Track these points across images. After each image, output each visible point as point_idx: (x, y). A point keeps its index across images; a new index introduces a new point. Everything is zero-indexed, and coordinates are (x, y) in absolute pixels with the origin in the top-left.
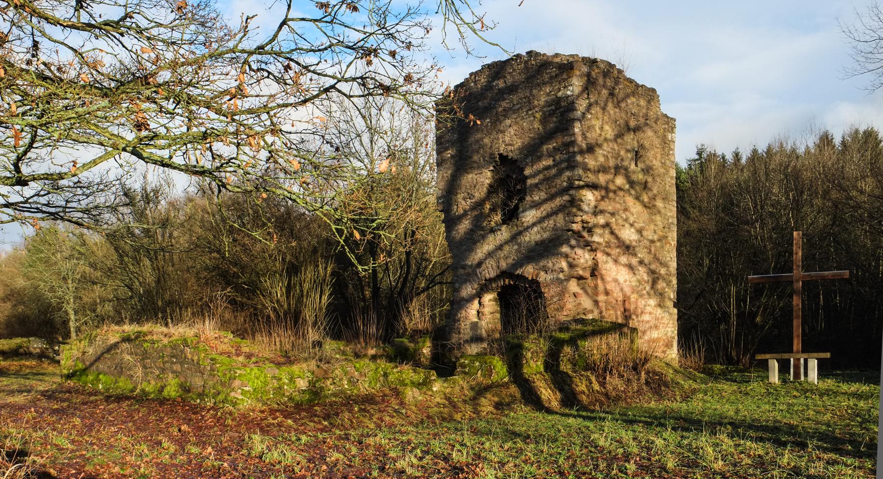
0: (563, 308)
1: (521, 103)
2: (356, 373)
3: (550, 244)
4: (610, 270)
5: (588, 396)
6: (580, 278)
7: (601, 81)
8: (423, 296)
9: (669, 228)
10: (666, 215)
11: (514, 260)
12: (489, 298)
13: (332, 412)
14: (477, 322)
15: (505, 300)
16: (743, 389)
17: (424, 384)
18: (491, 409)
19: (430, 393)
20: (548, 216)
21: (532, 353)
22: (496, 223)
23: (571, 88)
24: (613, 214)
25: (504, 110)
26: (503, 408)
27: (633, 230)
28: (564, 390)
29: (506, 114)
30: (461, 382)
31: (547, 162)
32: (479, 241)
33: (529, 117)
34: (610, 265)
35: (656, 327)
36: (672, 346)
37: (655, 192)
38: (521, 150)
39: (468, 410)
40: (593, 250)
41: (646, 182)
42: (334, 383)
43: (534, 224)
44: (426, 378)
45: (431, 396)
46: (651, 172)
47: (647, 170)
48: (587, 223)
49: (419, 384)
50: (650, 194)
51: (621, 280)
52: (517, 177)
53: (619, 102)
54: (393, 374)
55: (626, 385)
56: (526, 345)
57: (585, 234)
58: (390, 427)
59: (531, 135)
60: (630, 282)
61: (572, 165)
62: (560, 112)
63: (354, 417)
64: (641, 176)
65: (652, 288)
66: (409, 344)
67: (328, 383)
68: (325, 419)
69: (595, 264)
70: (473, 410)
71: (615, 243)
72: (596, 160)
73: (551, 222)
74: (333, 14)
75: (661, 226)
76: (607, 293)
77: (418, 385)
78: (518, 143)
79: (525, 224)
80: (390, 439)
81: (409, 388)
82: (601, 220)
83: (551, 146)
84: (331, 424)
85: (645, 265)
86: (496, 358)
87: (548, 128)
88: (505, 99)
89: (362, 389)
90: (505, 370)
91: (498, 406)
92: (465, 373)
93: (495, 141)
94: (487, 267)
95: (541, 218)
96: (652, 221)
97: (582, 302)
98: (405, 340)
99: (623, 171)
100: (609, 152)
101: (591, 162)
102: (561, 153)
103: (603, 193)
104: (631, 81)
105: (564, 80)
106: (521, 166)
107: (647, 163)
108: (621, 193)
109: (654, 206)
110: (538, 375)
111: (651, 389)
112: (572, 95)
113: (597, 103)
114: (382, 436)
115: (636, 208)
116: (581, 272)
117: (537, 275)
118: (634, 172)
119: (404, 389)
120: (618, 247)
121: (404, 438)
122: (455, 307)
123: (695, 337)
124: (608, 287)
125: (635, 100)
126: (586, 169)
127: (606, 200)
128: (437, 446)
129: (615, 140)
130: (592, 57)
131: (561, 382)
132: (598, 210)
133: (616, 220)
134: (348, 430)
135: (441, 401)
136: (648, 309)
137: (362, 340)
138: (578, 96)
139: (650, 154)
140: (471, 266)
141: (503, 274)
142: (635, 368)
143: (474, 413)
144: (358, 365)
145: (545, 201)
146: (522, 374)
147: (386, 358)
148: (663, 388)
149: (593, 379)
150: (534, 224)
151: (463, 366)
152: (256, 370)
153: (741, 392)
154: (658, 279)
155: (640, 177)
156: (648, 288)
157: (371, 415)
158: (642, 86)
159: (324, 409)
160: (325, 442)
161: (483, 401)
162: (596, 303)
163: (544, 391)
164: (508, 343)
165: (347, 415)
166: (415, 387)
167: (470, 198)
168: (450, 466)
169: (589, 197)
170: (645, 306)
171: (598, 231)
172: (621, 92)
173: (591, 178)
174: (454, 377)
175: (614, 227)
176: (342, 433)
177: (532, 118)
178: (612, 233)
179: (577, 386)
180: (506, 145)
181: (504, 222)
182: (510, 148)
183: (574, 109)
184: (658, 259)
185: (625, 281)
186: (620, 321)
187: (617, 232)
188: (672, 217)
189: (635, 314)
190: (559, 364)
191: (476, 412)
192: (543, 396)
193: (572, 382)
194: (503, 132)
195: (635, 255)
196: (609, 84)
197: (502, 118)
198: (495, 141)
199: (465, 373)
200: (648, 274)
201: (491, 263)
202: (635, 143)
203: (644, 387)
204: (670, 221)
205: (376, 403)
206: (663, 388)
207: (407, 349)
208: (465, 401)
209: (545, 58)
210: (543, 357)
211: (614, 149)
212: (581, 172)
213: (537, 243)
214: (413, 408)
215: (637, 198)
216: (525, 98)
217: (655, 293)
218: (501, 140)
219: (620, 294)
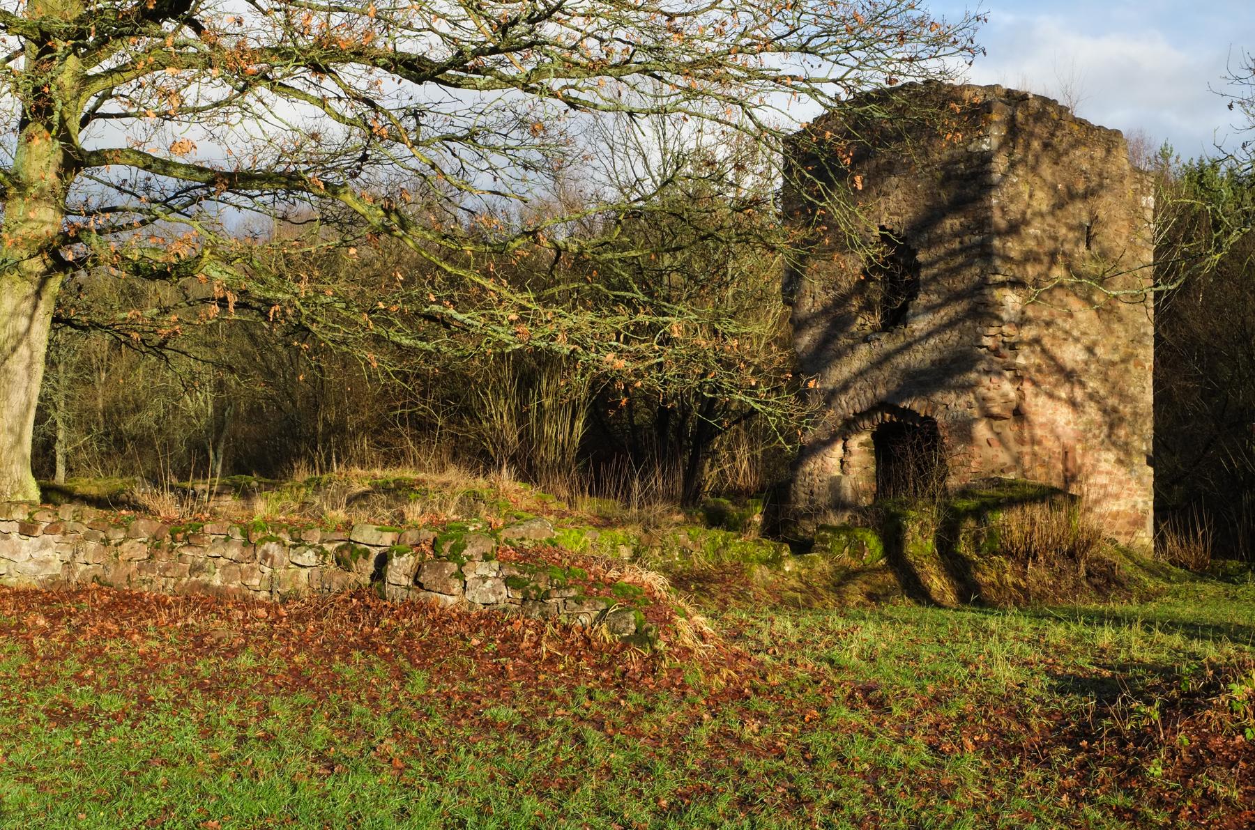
4: (1043, 407)
5: (999, 591)
10: (1134, 321)
12: (859, 442)
14: (840, 478)
15: (883, 445)
17: (774, 563)
18: (860, 598)
20: (951, 324)
30: (822, 562)
32: (846, 355)
34: (1042, 399)
36: (1143, 525)
43: (929, 335)
53: (1060, 155)
60: (1076, 424)
61: (985, 253)
76: (1034, 441)
77: (766, 562)
79: (917, 334)
89: (696, 564)
92: (826, 550)
96: (1111, 331)
101: (1014, 248)
104: (1082, 123)
106: (912, 247)
107: (1106, 244)
108: (1058, 294)
113: (1023, 161)
115: (1084, 315)
123: (1195, 512)
126: (1007, 259)
129: (1052, 213)
131: (958, 570)
136: (1104, 466)
144: (692, 532)
150: (929, 335)
152: (575, 533)
153: (1227, 595)
155: (1090, 267)
169: (1011, 300)
175: (1047, 342)
178: (1044, 351)
180: (891, 214)
185: (1068, 423)
186: (1056, 483)
193: (978, 569)
194: (886, 194)
199: (826, 550)
208: (826, 588)
213: (933, 363)
215: (1088, 300)
218: (883, 206)
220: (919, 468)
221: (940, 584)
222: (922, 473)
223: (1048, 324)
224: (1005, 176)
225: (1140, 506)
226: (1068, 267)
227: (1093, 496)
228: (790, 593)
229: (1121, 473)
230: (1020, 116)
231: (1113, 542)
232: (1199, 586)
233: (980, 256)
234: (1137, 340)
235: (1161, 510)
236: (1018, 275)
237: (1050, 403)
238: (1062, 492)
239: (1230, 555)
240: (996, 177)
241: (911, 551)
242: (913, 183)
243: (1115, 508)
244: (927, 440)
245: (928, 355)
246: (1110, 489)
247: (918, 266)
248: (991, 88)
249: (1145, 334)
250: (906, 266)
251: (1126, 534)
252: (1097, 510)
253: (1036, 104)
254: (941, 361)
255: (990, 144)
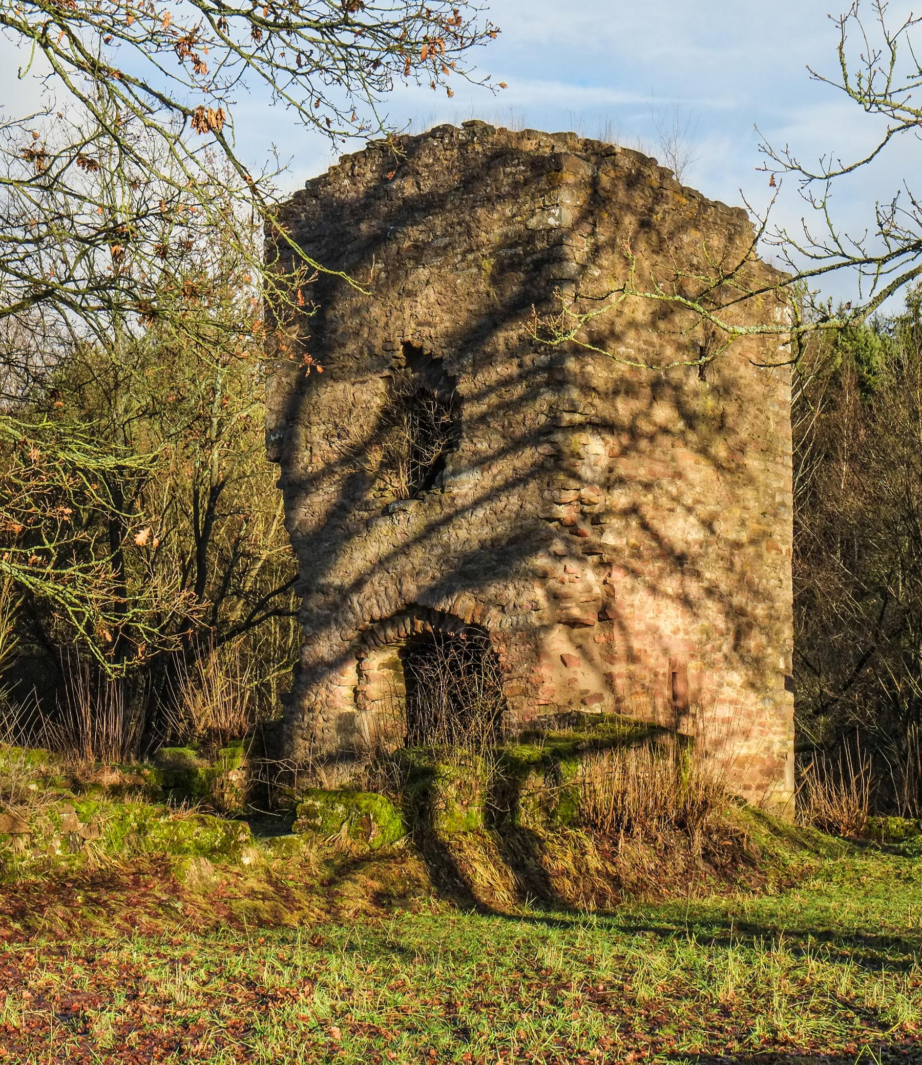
0: (536, 688)
1: (451, 235)
2: (81, 825)
3: (511, 548)
4: (641, 608)
5: (575, 881)
6: (573, 623)
7: (621, 194)
8: (236, 643)
9: (775, 515)
10: (767, 486)
11: (433, 578)
13: (29, 905)
16: (904, 869)
18: (363, 904)
19: (236, 869)
20: (509, 486)
21: (459, 788)
22: (396, 494)
23: (556, 212)
24: (647, 487)
25: (416, 247)
26: (390, 903)
27: (692, 519)
28: (525, 866)
29: (419, 253)
30: (304, 848)
31: (504, 370)
32: (358, 533)
33: (469, 267)
34: (642, 596)
35: (746, 734)
36: (781, 774)
37: (744, 435)
38: (450, 338)
39: (315, 907)
40: (605, 565)
41: (723, 416)
42: (34, 845)
43: (477, 503)
44: (230, 836)
45: (238, 874)
46: (735, 391)
47: (724, 390)
48: (591, 503)
49: (213, 850)
50: (732, 441)
51: (666, 628)
52: (443, 395)
54: (159, 827)
55: (662, 859)
56: (444, 769)
57: (586, 528)
58: (150, 936)
59: (471, 307)
60: (687, 633)
62: (533, 262)
63: (75, 915)
64: (710, 402)
65: (736, 647)
66: (196, 761)
67: (22, 843)
68: (14, 917)
69: (608, 594)
70: (326, 906)
71: (653, 549)
72: (609, 367)
73: (514, 500)
74: (54, 171)
75: (756, 512)
76: (632, 657)
77: (211, 852)
78: (444, 323)
79: (459, 502)
80: (149, 955)
81: (191, 859)
82: (620, 498)
83: (514, 334)
84: (27, 928)
85: (721, 596)
86: (380, 797)
87: (508, 294)
88: (415, 223)
90: (398, 823)
91: (381, 899)
92: (315, 828)
93: (395, 313)
94: (376, 593)
95: (492, 489)
97: (579, 676)
98: (190, 754)
99: (669, 392)
100: (640, 350)
102: (536, 352)
103: (625, 440)
104: (691, 194)
105: (543, 192)
107: (727, 372)
108: (665, 441)
109: (741, 467)
110: (470, 836)
111: (716, 867)
112: (560, 227)
113: (612, 244)
114: (138, 122)
116: (576, 612)
117: (483, 616)
118: (696, 394)
119: (181, 860)
120: (658, 557)
121: (176, 953)
122: (304, 678)
123: (848, 751)
124: (636, 644)
125: (699, 235)
126: (587, 388)
127: (633, 454)
128: (237, 965)
129: (653, 325)
130: (606, 141)
132: (613, 477)
133: (655, 498)
134: (62, 940)
135: (257, 887)
136: (728, 693)
137: (88, 749)
138: (572, 230)
139: (733, 354)
140: (340, 589)
141: (410, 609)
142: (681, 824)
143: (328, 912)
144: (83, 809)
145: (502, 453)
146: (433, 835)
147: (145, 793)
148: (741, 866)
149: (589, 845)
150: (477, 503)
151: (311, 813)
153: (898, 876)
154: (750, 626)
155: (707, 404)
156: (726, 648)
157: (112, 912)
158: (716, 204)
159: (11, 898)
160: (20, 959)
161: (348, 887)
162: (609, 680)
163: (480, 869)
164: (406, 766)
165: (60, 909)
166: (205, 856)
167: (339, 436)
168: (257, 994)
170: (720, 685)
171: (616, 522)
172: (668, 218)
173: (600, 408)
174: (290, 836)
175: (648, 512)
176: (53, 944)
177: (475, 270)
178: (645, 526)
179: (554, 858)
180: (419, 324)
181: (414, 494)
182: (426, 330)
183: (561, 259)
184: (750, 584)
185: (676, 632)
186: (662, 719)
187: (656, 524)
188: (782, 491)
189: (697, 705)
190: (518, 811)
191: (333, 912)
192: (478, 880)
193: (544, 850)
194: (411, 294)
195: (698, 575)
196: (641, 202)
197: (410, 264)
198: (395, 313)
199: (315, 828)
200: (727, 614)
201: (380, 583)
202: (699, 329)
203: (700, 863)
204: (778, 499)
205: (122, 888)
206: (741, 866)
207: (191, 772)
208: (310, 888)
209: (503, 139)
210: (481, 795)
211: (652, 344)
212: (575, 394)
213: (482, 543)
214: (200, 899)
215: (703, 451)
216: (459, 224)
217: (742, 657)
218: (408, 312)
219: (663, 661)
220: (455, 701)
221: (486, 875)
222: (460, 706)
223: (647, 487)
224: (583, 267)
225: (776, 748)
226: (679, 405)
227: (712, 735)
228: (246, 901)
229: (751, 700)
230: (605, 181)
231: (741, 802)
232: (859, 863)
233: (547, 384)
234: (772, 513)
235: (803, 749)
236: (606, 414)
237: (650, 600)
238: (672, 729)
239: (889, 808)
240: (572, 267)
241: (444, 825)
242: (451, 277)
243: (744, 752)
244: (467, 658)
245: (473, 532)
246: (734, 725)
247: (458, 402)
248: (561, 137)
249: (783, 504)
250: (441, 401)
251: (759, 787)
252: (720, 755)
253: (625, 163)
254: (495, 541)
255: (559, 218)
